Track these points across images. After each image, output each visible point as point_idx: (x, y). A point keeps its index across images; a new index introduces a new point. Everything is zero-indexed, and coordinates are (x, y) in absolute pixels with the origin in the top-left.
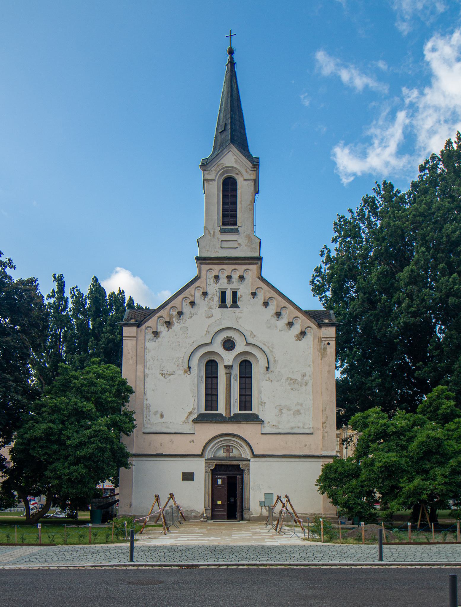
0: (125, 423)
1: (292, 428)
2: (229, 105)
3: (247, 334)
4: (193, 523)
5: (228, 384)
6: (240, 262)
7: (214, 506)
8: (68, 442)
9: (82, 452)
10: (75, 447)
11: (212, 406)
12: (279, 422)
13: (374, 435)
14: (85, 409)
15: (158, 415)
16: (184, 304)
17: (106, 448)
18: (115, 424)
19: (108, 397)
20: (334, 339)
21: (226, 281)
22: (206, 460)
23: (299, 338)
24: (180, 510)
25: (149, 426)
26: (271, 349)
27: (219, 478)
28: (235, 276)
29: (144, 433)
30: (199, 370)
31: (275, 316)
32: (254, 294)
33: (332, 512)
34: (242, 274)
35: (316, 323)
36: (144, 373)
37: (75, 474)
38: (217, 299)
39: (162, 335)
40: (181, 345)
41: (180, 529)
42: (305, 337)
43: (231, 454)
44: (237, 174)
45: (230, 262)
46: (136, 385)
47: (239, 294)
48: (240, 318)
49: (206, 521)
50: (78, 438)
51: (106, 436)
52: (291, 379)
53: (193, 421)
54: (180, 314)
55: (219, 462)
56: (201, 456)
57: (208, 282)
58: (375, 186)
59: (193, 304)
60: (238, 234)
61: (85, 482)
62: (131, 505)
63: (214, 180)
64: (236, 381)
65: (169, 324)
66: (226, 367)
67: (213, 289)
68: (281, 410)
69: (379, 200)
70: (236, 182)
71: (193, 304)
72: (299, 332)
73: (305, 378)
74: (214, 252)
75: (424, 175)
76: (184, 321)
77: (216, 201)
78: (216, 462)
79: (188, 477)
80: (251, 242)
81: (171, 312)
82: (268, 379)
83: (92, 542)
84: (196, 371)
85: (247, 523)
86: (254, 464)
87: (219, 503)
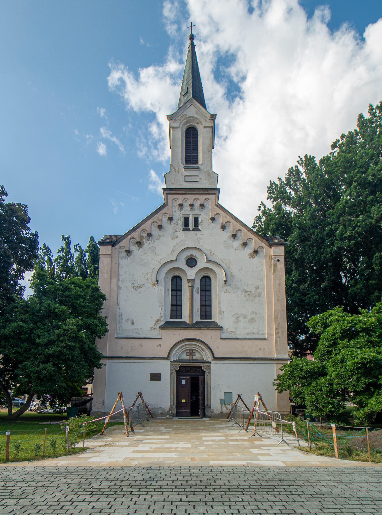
0: (97, 326)
1: (248, 334)
2: (191, 74)
3: (208, 253)
4: (159, 421)
5: (191, 296)
6: (200, 192)
7: (179, 404)
8: (38, 340)
9: (51, 351)
10: (45, 345)
11: (176, 315)
12: (236, 329)
13: (340, 333)
14: (57, 310)
15: (130, 322)
16: (153, 228)
17: (74, 346)
18: (88, 327)
19: (81, 302)
20: (283, 257)
21: (189, 208)
22: (171, 362)
23: (252, 256)
24: (147, 407)
25: (121, 332)
26: (228, 265)
27: (184, 379)
28: (197, 205)
29: (116, 338)
30: (166, 284)
31: (231, 238)
32: (213, 219)
33: (286, 410)
34: (202, 203)
35: (267, 243)
36: (118, 285)
37: (44, 372)
38: (181, 223)
39: (134, 254)
40: (150, 262)
41: (145, 429)
42: (258, 255)
43: (194, 357)
44: (198, 123)
45: (193, 192)
46: (110, 297)
47: (200, 220)
48: (201, 239)
49: (172, 418)
50: (48, 337)
51: (74, 335)
52: (246, 291)
53: (160, 327)
54: (149, 235)
55: (183, 364)
56: (167, 358)
57: (174, 210)
58: (299, 159)
59: (160, 227)
60: (199, 170)
61: (55, 380)
62: (103, 403)
63: (179, 127)
64: (198, 293)
65: (140, 244)
66: (189, 280)
67: (178, 215)
68: (237, 318)
69: (302, 169)
70: (197, 131)
71: (160, 227)
72: (252, 251)
73: (258, 290)
74: (179, 185)
75: (335, 152)
76: (153, 241)
77: (181, 144)
78: (180, 364)
79: (155, 377)
80: (210, 176)
81: (142, 234)
82: (226, 291)
83: (11, 457)
84: (163, 284)
85: (210, 420)
86: (215, 366)
87: (183, 401)
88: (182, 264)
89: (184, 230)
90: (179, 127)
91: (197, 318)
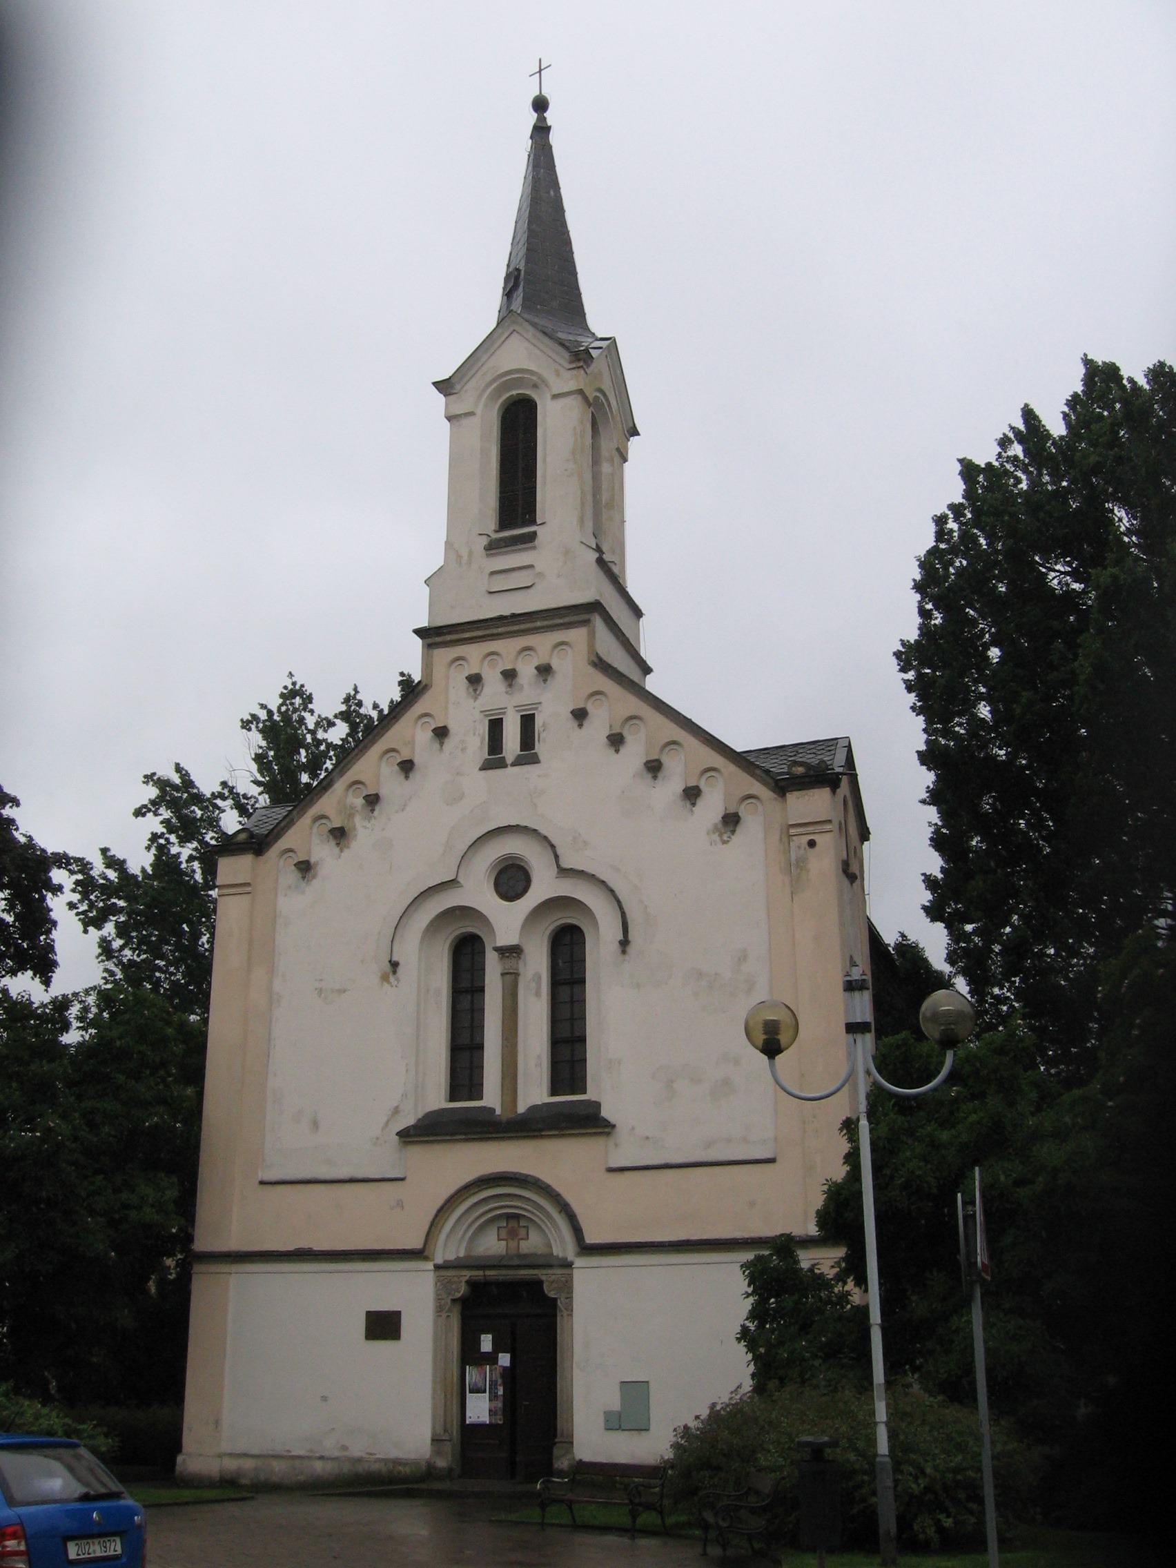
1: (709, 1145)
22: (437, 1267)
28: (526, 671)
44: (535, 386)
47: (539, 722)
52: (700, 974)
62: (217, 1423)
63: (472, 414)
64: (538, 994)
65: (340, 835)
78: (467, 1274)
79: (383, 1326)
88: (478, 892)
89: (487, 766)
90: (472, 414)
91: (535, 1091)
